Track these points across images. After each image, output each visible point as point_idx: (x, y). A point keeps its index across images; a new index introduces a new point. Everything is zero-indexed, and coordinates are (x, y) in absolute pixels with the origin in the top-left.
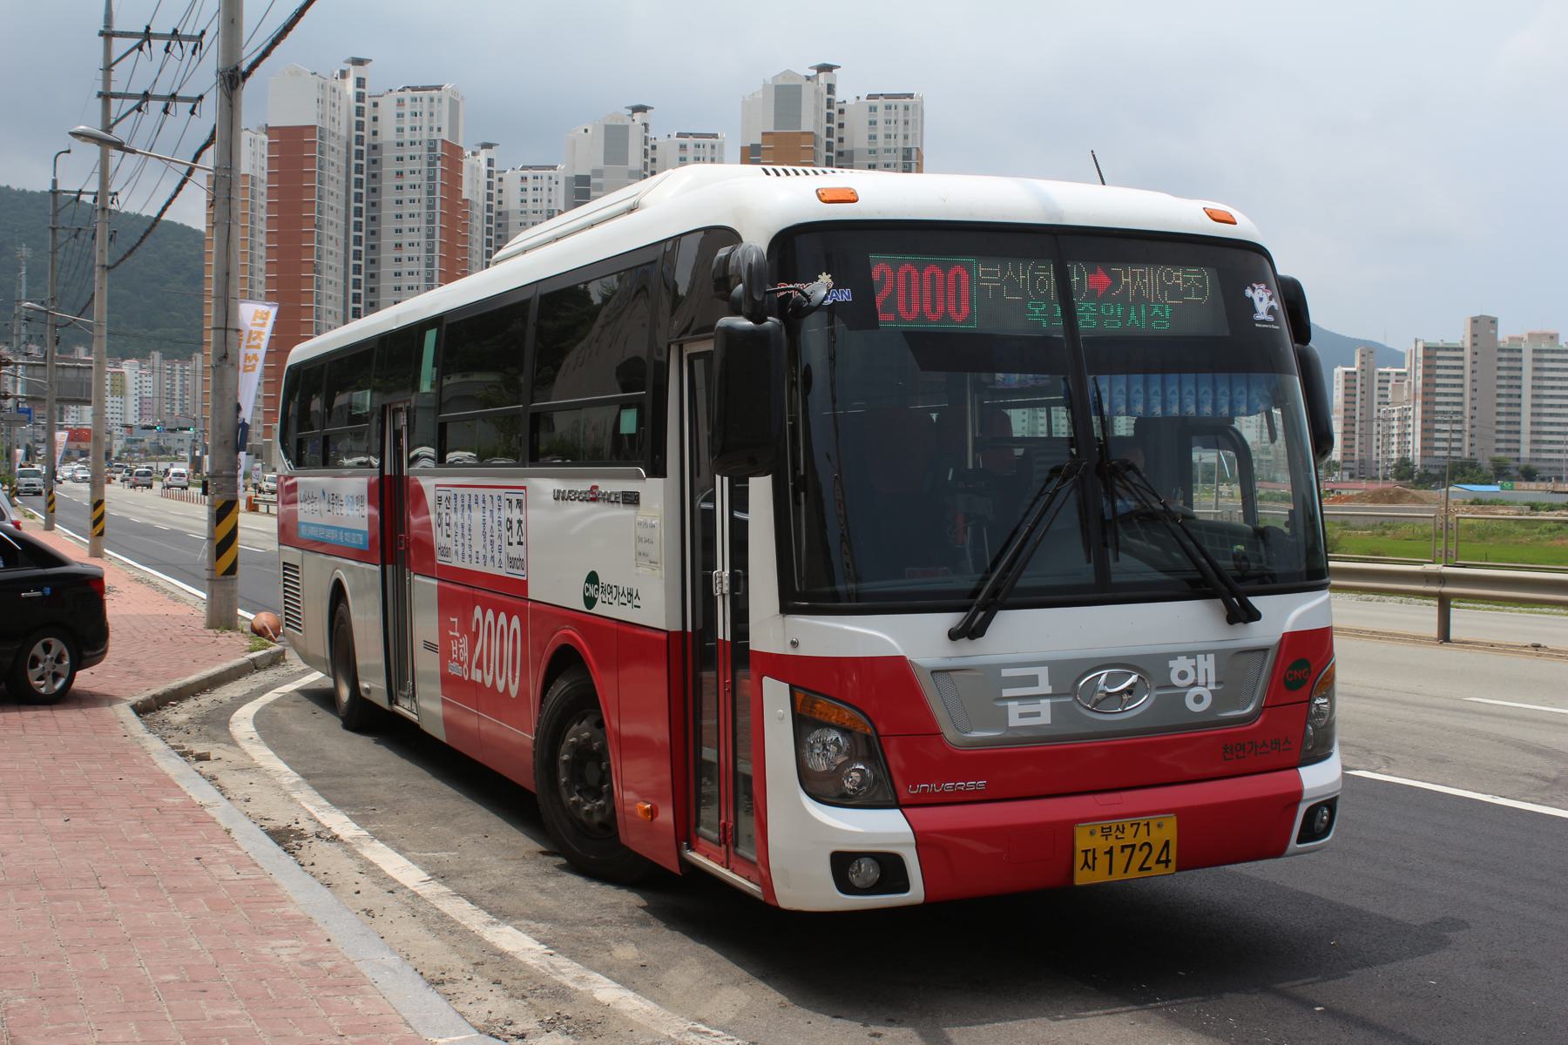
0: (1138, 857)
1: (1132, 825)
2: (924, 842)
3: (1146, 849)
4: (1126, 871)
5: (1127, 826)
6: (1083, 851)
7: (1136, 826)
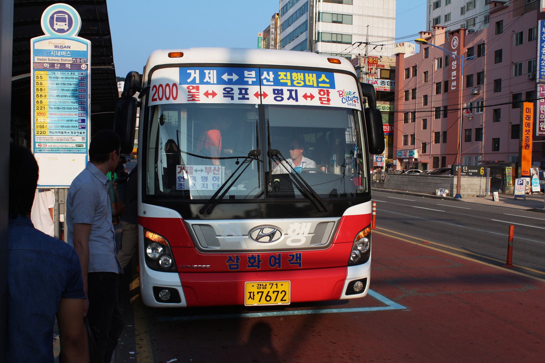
0: (280, 296)
1: (270, 284)
2: (184, 285)
3: (284, 293)
4: (260, 301)
5: (268, 284)
6: (249, 292)
7: (272, 285)
